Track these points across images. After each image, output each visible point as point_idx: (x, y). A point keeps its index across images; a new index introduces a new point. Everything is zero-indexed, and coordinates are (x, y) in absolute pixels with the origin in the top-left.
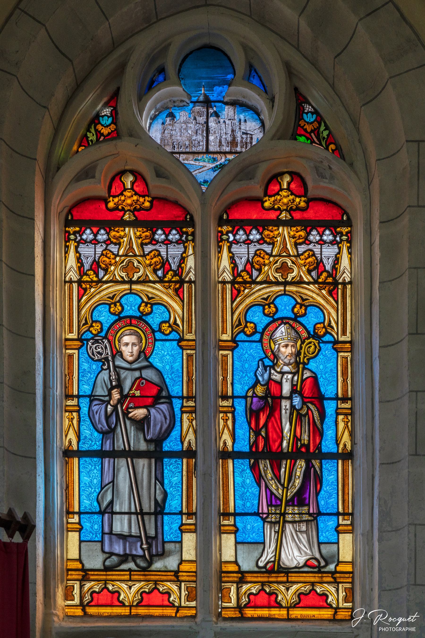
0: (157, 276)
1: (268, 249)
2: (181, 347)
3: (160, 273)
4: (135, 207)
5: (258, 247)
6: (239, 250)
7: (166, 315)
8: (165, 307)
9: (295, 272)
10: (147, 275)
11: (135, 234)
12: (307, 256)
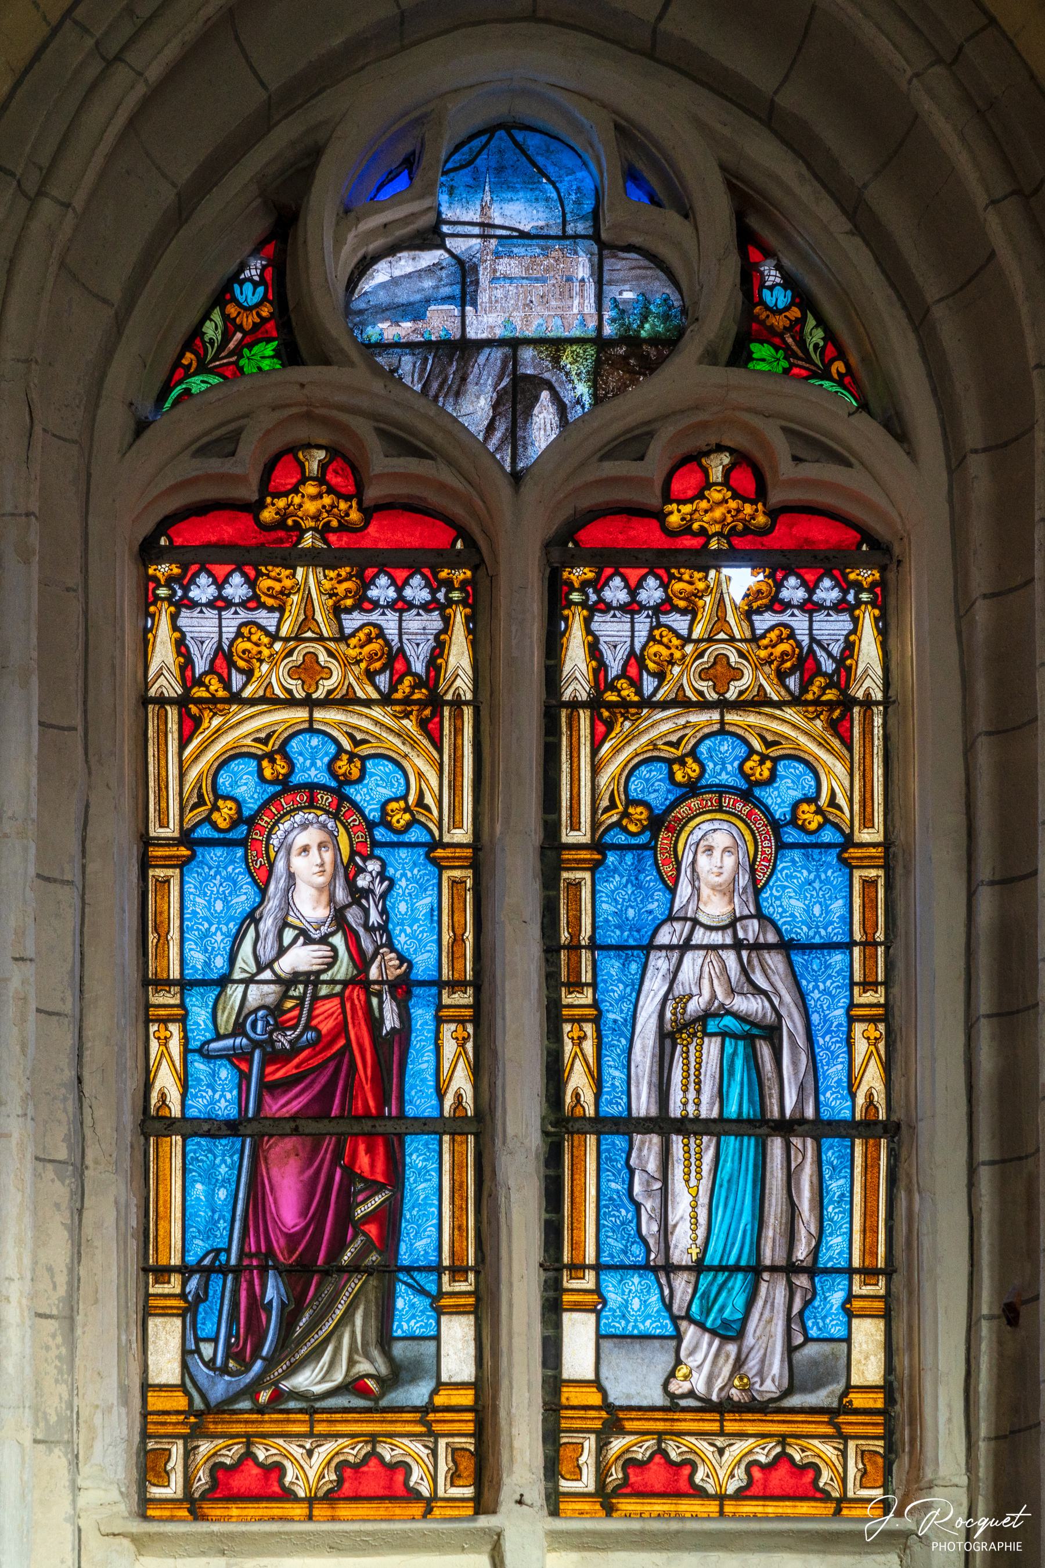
0: (787, 688)
1: (268, 620)
2: (434, 861)
3: (792, 682)
4: (734, 528)
5: (244, 615)
6: (195, 622)
7: (809, 780)
8: (807, 763)
9: (335, 673)
10: (761, 685)
11: (319, 583)
12: (775, 639)
